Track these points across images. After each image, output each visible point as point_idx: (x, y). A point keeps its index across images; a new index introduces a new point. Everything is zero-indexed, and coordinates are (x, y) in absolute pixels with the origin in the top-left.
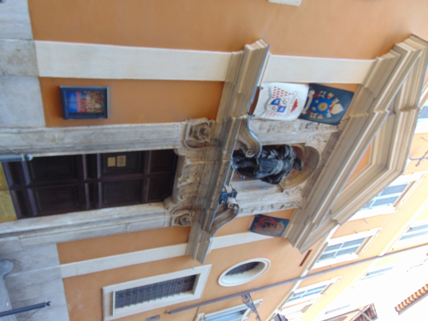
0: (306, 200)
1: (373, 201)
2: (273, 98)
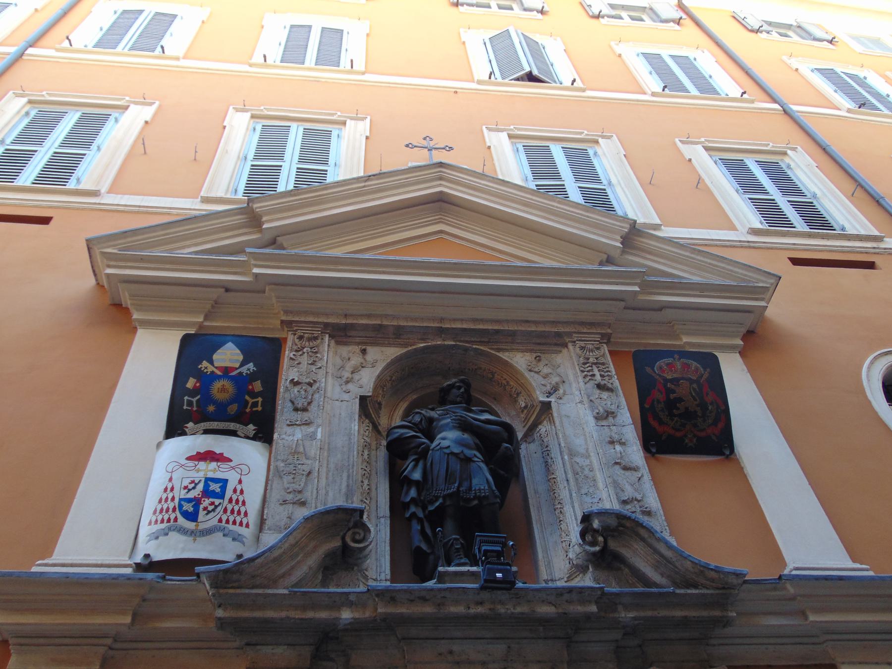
0: (570, 334)
1: (537, 186)
2: (176, 519)
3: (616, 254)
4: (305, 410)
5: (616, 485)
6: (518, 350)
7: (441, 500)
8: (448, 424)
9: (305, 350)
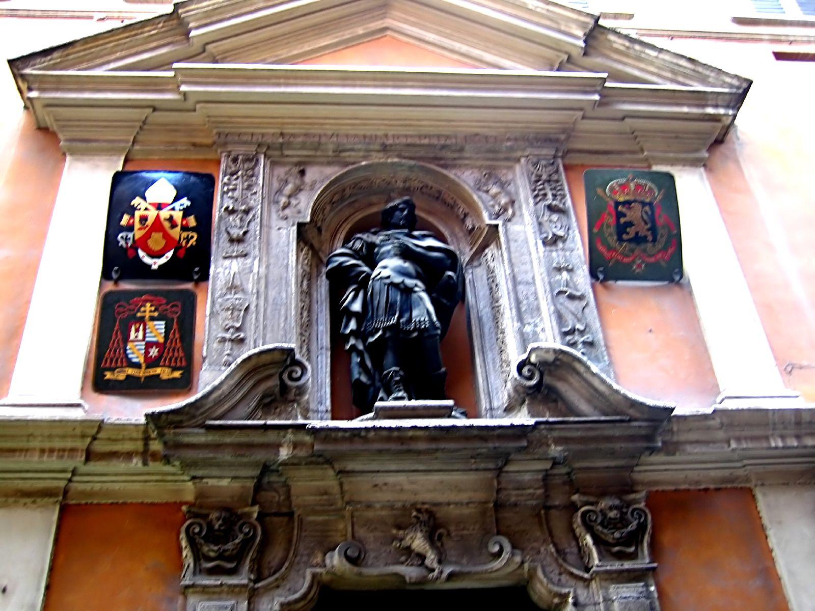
3: (577, 53)
4: (240, 240)
5: (560, 317)
7: (380, 333)
8: (389, 251)
9: (240, 173)
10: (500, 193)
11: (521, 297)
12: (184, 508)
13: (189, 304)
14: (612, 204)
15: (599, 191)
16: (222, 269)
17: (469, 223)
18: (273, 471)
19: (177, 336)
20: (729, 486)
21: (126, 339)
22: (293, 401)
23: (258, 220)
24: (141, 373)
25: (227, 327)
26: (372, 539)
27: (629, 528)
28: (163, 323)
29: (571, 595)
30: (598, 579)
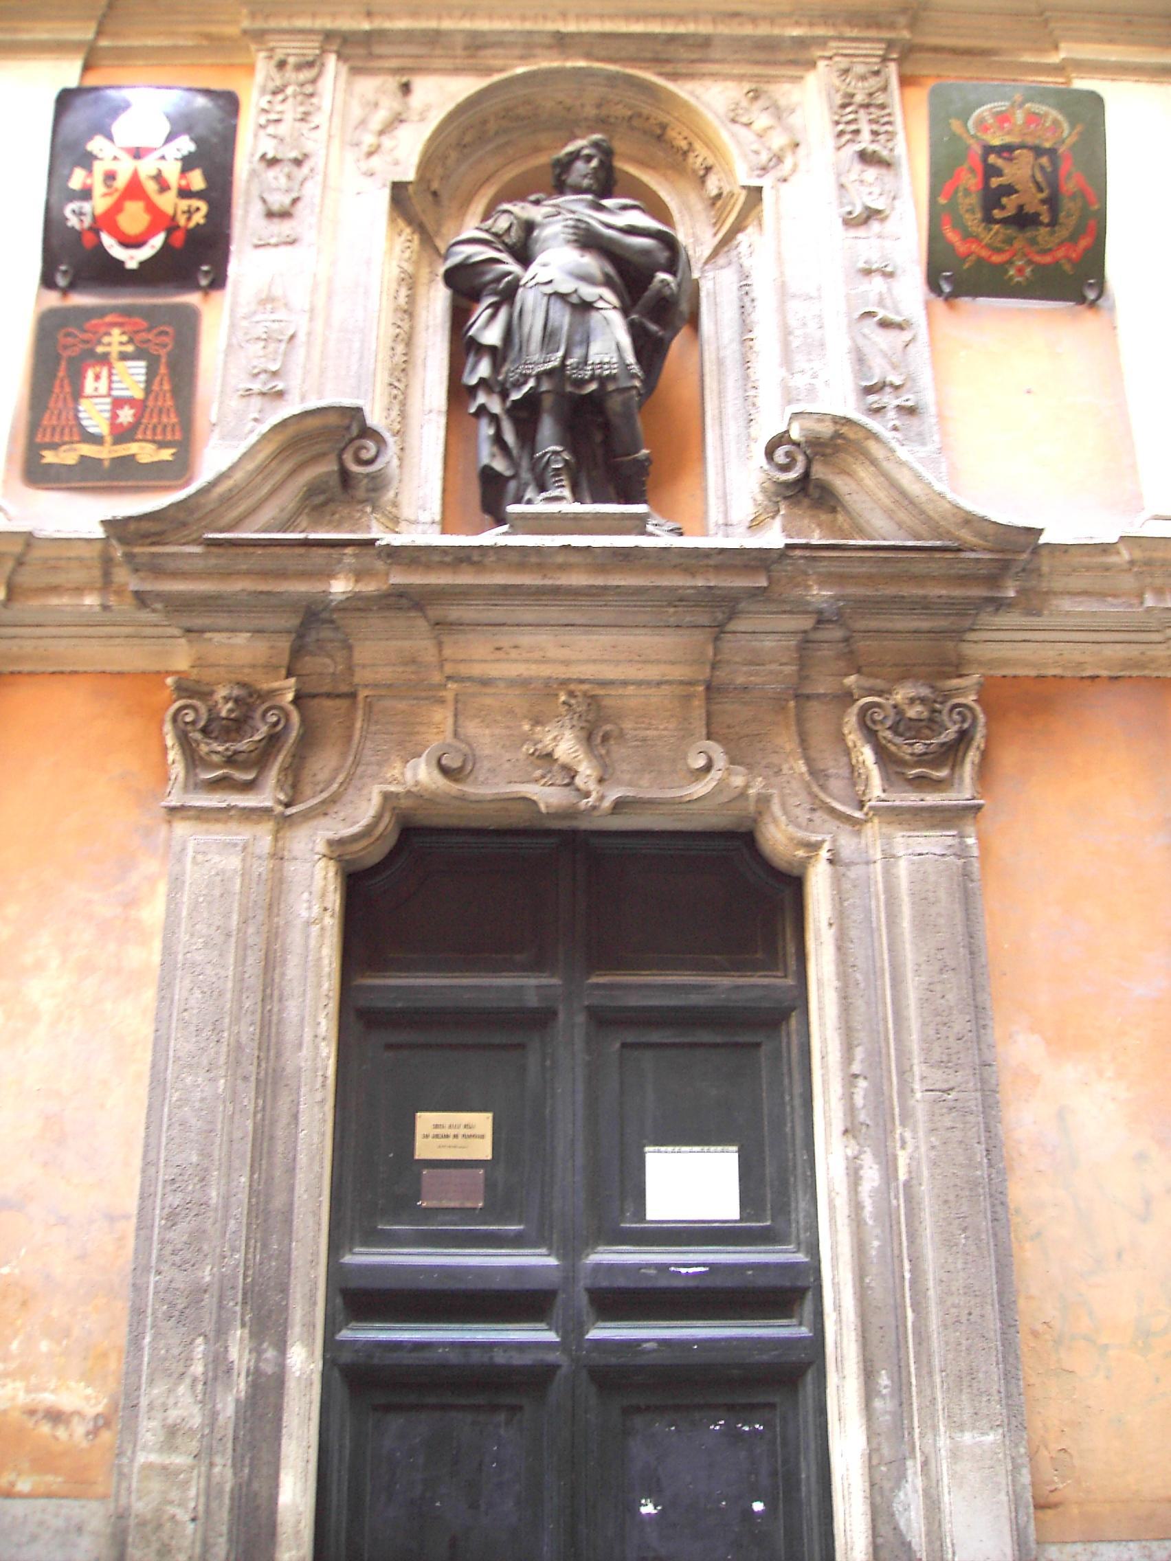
4: (285, 215)
5: (860, 360)
6: (714, 76)
7: (531, 383)
8: (555, 236)
10: (771, 128)
11: (793, 322)
12: (170, 681)
13: (186, 331)
14: (978, 150)
15: (955, 125)
16: (244, 264)
17: (712, 185)
18: (325, 621)
19: (166, 387)
20: (1135, 673)
21: (77, 393)
22: (365, 501)
23: (319, 178)
24: (105, 453)
25: (256, 371)
26: (488, 740)
27: (943, 738)
28: (143, 364)
29: (826, 846)
30: (876, 820)
